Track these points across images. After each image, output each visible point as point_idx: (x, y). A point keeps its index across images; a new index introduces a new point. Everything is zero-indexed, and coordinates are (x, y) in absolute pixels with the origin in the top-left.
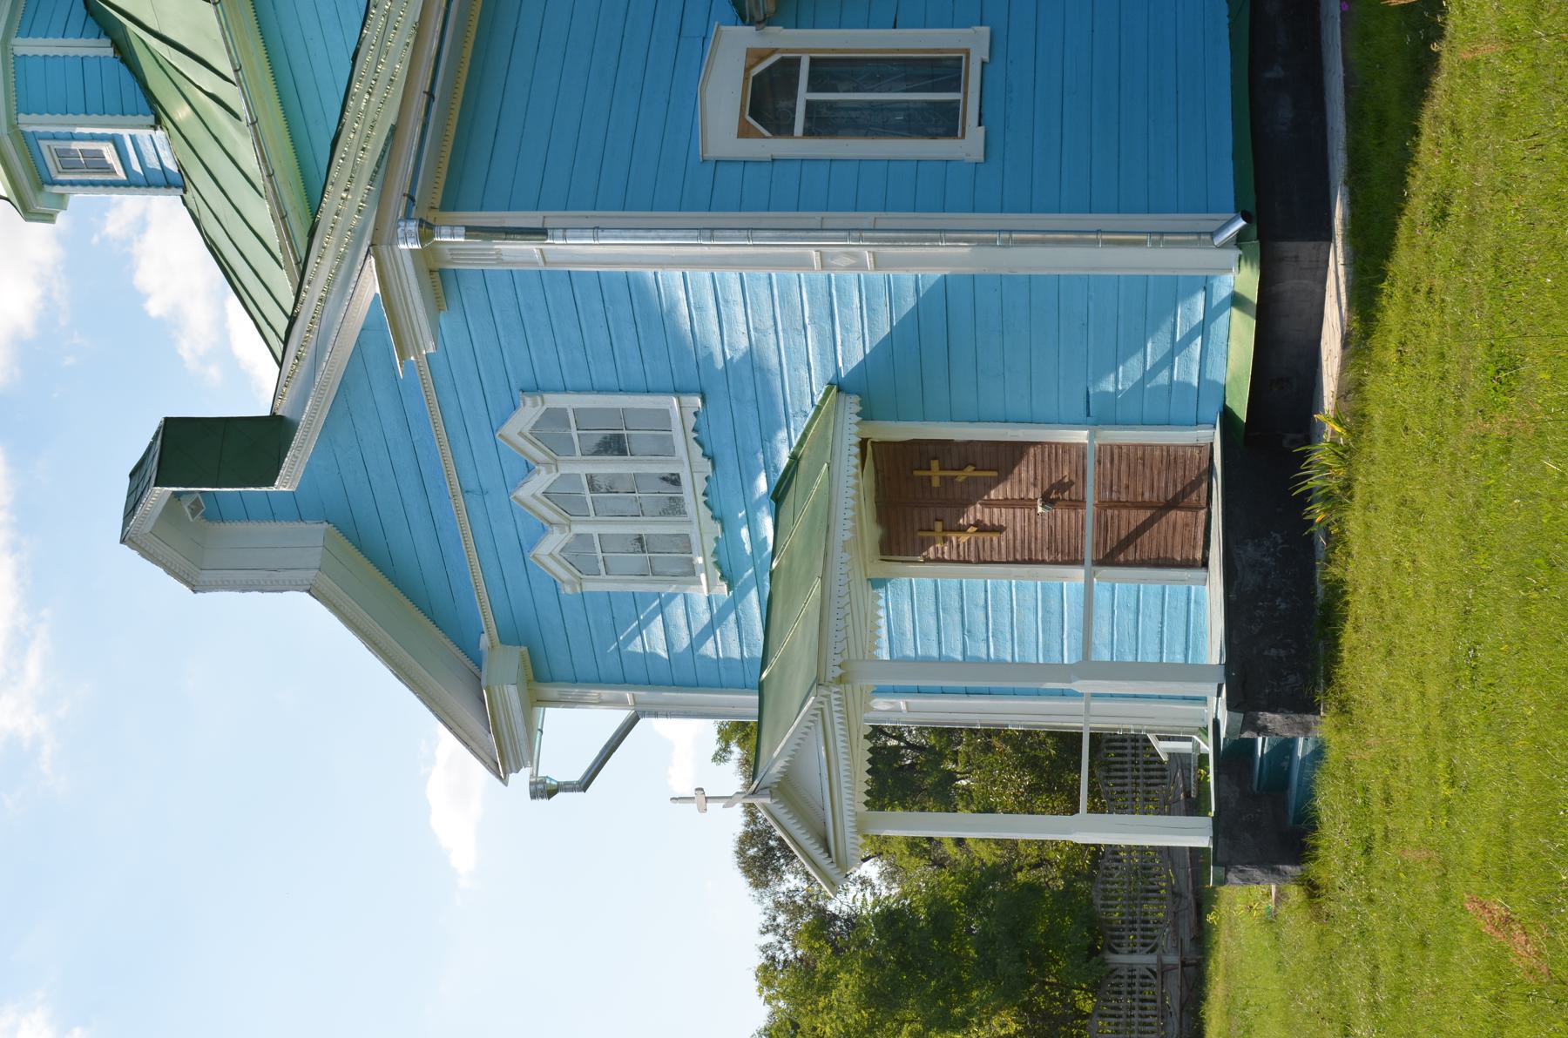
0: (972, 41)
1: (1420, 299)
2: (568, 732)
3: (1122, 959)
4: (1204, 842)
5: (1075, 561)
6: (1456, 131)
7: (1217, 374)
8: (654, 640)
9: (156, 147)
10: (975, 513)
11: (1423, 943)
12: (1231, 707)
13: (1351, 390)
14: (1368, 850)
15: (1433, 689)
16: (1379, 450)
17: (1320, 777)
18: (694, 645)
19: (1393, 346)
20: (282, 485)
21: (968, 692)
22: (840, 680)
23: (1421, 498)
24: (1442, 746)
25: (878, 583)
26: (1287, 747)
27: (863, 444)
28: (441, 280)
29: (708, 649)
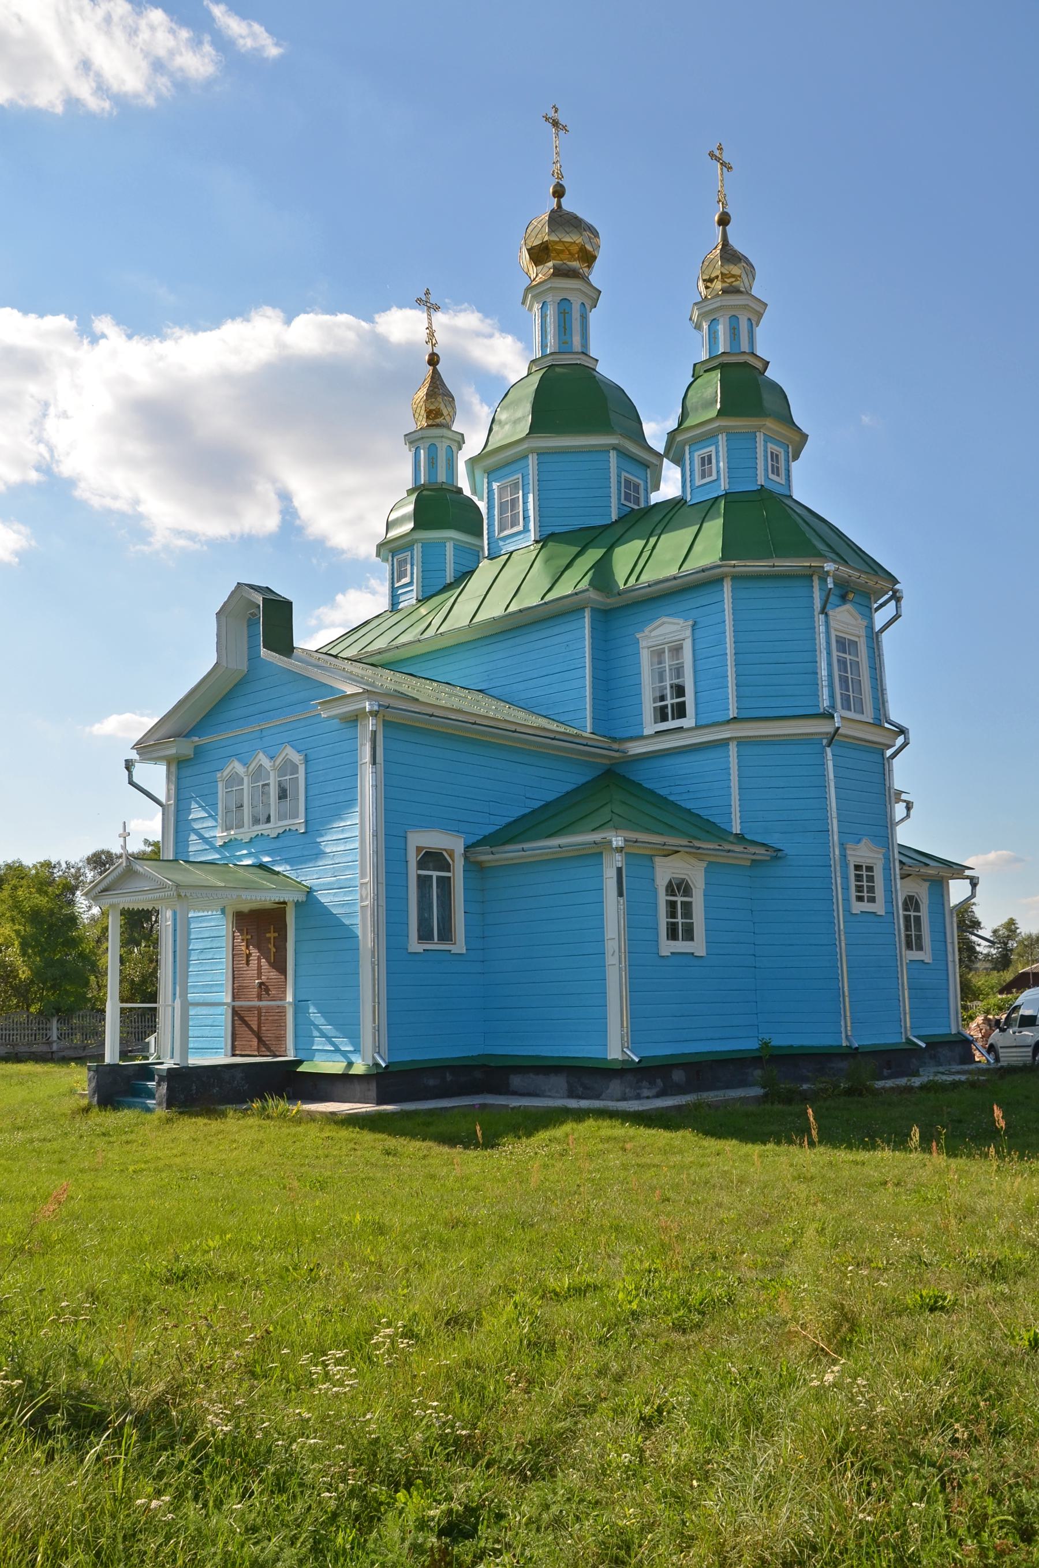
0: (459, 946)
1: (351, 1145)
2: (155, 776)
4: (108, 1060)
5: (234, 998)
6: (425, 1157)
7: (318, 1057)
8: (197, 813)
9: (408, 600)
10: (255, 953)
11: (61, 1162)
13: (312, 1117)
14: (104, 1134)
15: (178, 1160)
20: (263, 652)
22: (179, 896)
23: (263, 1151)
24: (152, 1166)
25: (223, 911)
26: (151, 1095)
27: (284, 903)
28: (353, 719)
29: (193, 837)
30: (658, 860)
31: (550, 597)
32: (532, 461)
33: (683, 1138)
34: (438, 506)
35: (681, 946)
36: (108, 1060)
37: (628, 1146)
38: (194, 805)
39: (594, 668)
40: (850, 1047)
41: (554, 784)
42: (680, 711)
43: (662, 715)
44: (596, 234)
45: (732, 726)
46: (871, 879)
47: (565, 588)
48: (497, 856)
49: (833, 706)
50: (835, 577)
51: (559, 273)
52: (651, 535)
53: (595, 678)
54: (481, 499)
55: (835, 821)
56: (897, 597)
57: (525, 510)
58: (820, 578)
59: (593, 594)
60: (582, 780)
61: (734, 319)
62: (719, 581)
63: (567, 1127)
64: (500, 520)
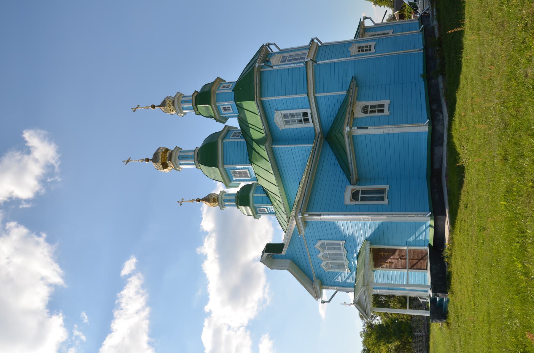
0: (386, 187)
1: (463, 222)
2: (326, 293)
3: (416, 333)
4: (429, 315)
5: (406, 268)
6: (468, 192)
7: (428, 238)
8: (339, 279)
9: (272, 209)
10: (389, 260)
11: (470, 335)
12: (432, 292)
13: (451, 239)
14: (458, 318)
15: (470, 289)
16: (457, 248)
17: (449, 305)
18: (346, 280)
19: (458, 230)
20: (283, 254)
21: (389, 289)
22: (367, 285)
23: (465, 256)
24: (472, 299)
25: (374, 271)
26: (442, 300)
27: (370, 249)
28: (306, 223)
29: (348, 281)
30: (355, 116)
31: (268, 159)
32: (226, 167)
33: (459, 96)
34: (242, 199)
35: (386, 108)
36: (429, 315)
37: (463, 114)
38: (337, 280)
39: (292, 144)
40: (423, 49)
41: (330, 157)
42: (305, 114)
43: (307, 120)
44: (159, 148)
45: (310, 95)
46: (363, 47)
47: (264, 154)
48: (354, 173)
49: (303, 62)
50: (261, 63)
51: (170, 159)
52: (248, 126)
53: (295, 144)
54: (240, 184)
55: (342, 59)
56: (268, 45)
57: (242, 169)
58: (261, 69)
59: (267, 144)
60: (329, 147)
61: (182, 102)
62: (262, 102)
63: (455, 141)
64: (245, 177)
